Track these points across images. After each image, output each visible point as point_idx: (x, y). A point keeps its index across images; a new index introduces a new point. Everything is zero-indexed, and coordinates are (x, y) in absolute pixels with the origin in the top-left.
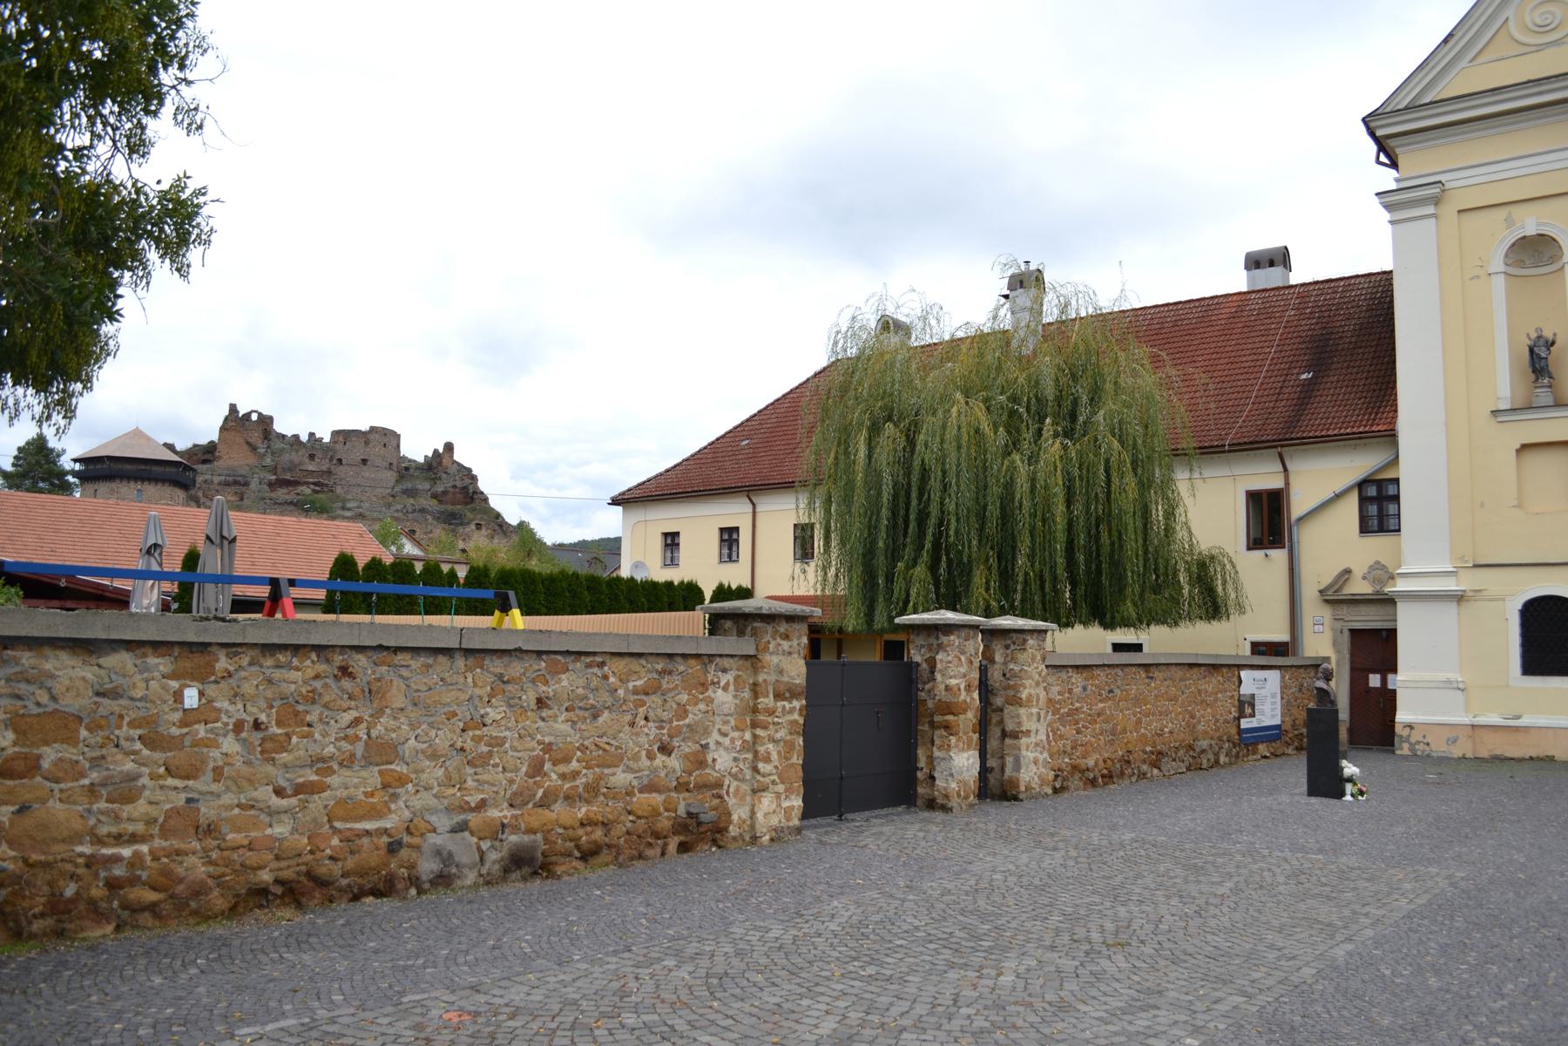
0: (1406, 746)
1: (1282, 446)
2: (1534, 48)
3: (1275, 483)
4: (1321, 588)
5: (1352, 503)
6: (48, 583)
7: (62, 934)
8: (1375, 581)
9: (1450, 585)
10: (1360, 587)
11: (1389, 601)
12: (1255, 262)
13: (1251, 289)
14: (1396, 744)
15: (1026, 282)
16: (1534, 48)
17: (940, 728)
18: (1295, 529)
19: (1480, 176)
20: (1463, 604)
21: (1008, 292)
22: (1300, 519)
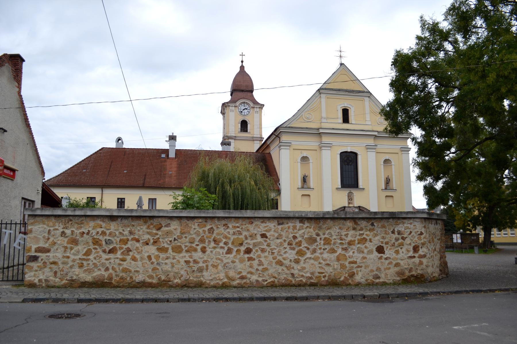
6: (55, 199)
7: (314, 251)
13: (223, 150)
15: (173, 138)
19: (297, 143)
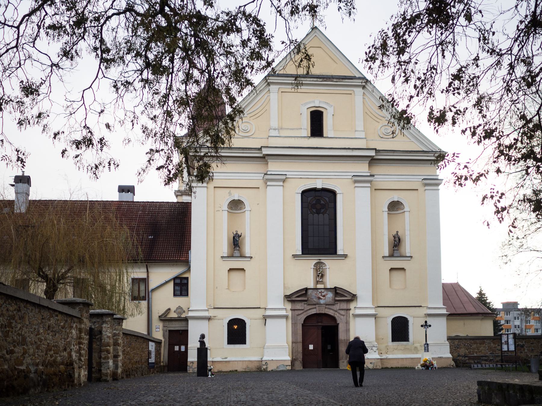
0: (191, 369)
1: (148, 262)
2: (241, 137)
3: (144, 276)
4: (160, 315)
5: (171, 285)
8: (178, 314)
9: (206, 314)
10: (173, 315)
11: (186, 320)
12: (122, 189)
14: (188, 369)
16: (241, 137)
17: (104, 351)
18: (150, 294)
20: (210, 321)
21: (14, 183)
22: (153, 290)
